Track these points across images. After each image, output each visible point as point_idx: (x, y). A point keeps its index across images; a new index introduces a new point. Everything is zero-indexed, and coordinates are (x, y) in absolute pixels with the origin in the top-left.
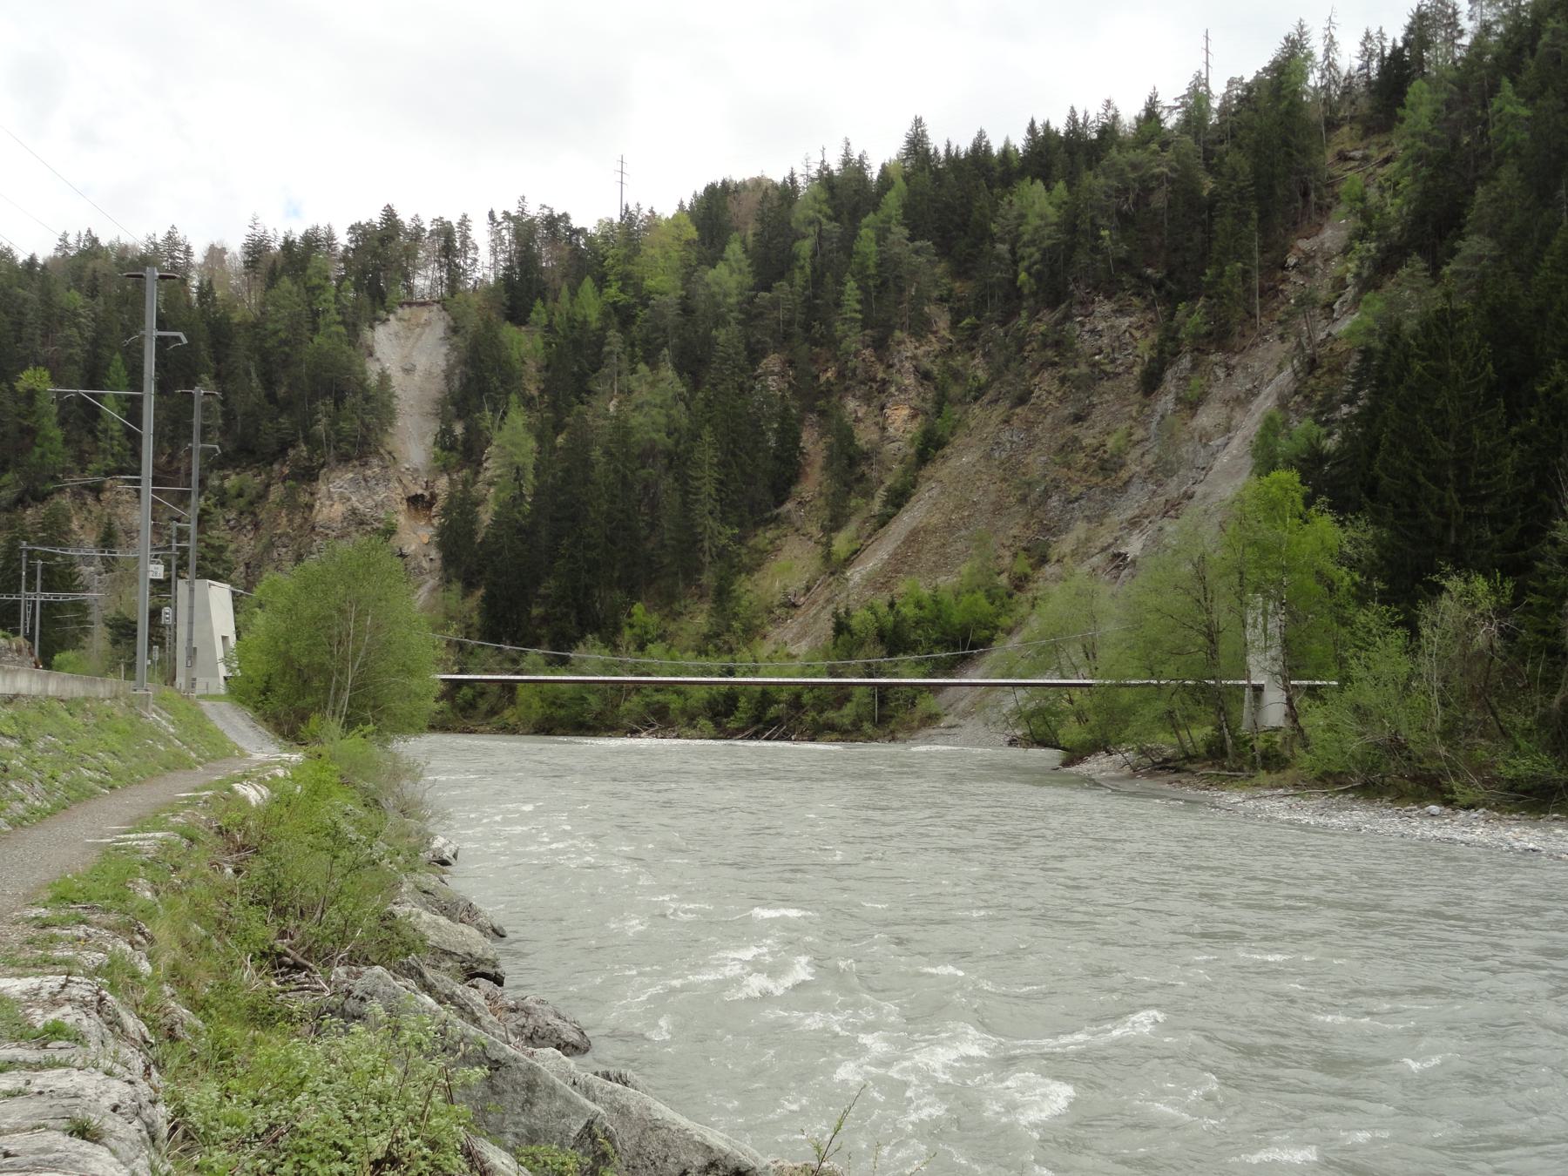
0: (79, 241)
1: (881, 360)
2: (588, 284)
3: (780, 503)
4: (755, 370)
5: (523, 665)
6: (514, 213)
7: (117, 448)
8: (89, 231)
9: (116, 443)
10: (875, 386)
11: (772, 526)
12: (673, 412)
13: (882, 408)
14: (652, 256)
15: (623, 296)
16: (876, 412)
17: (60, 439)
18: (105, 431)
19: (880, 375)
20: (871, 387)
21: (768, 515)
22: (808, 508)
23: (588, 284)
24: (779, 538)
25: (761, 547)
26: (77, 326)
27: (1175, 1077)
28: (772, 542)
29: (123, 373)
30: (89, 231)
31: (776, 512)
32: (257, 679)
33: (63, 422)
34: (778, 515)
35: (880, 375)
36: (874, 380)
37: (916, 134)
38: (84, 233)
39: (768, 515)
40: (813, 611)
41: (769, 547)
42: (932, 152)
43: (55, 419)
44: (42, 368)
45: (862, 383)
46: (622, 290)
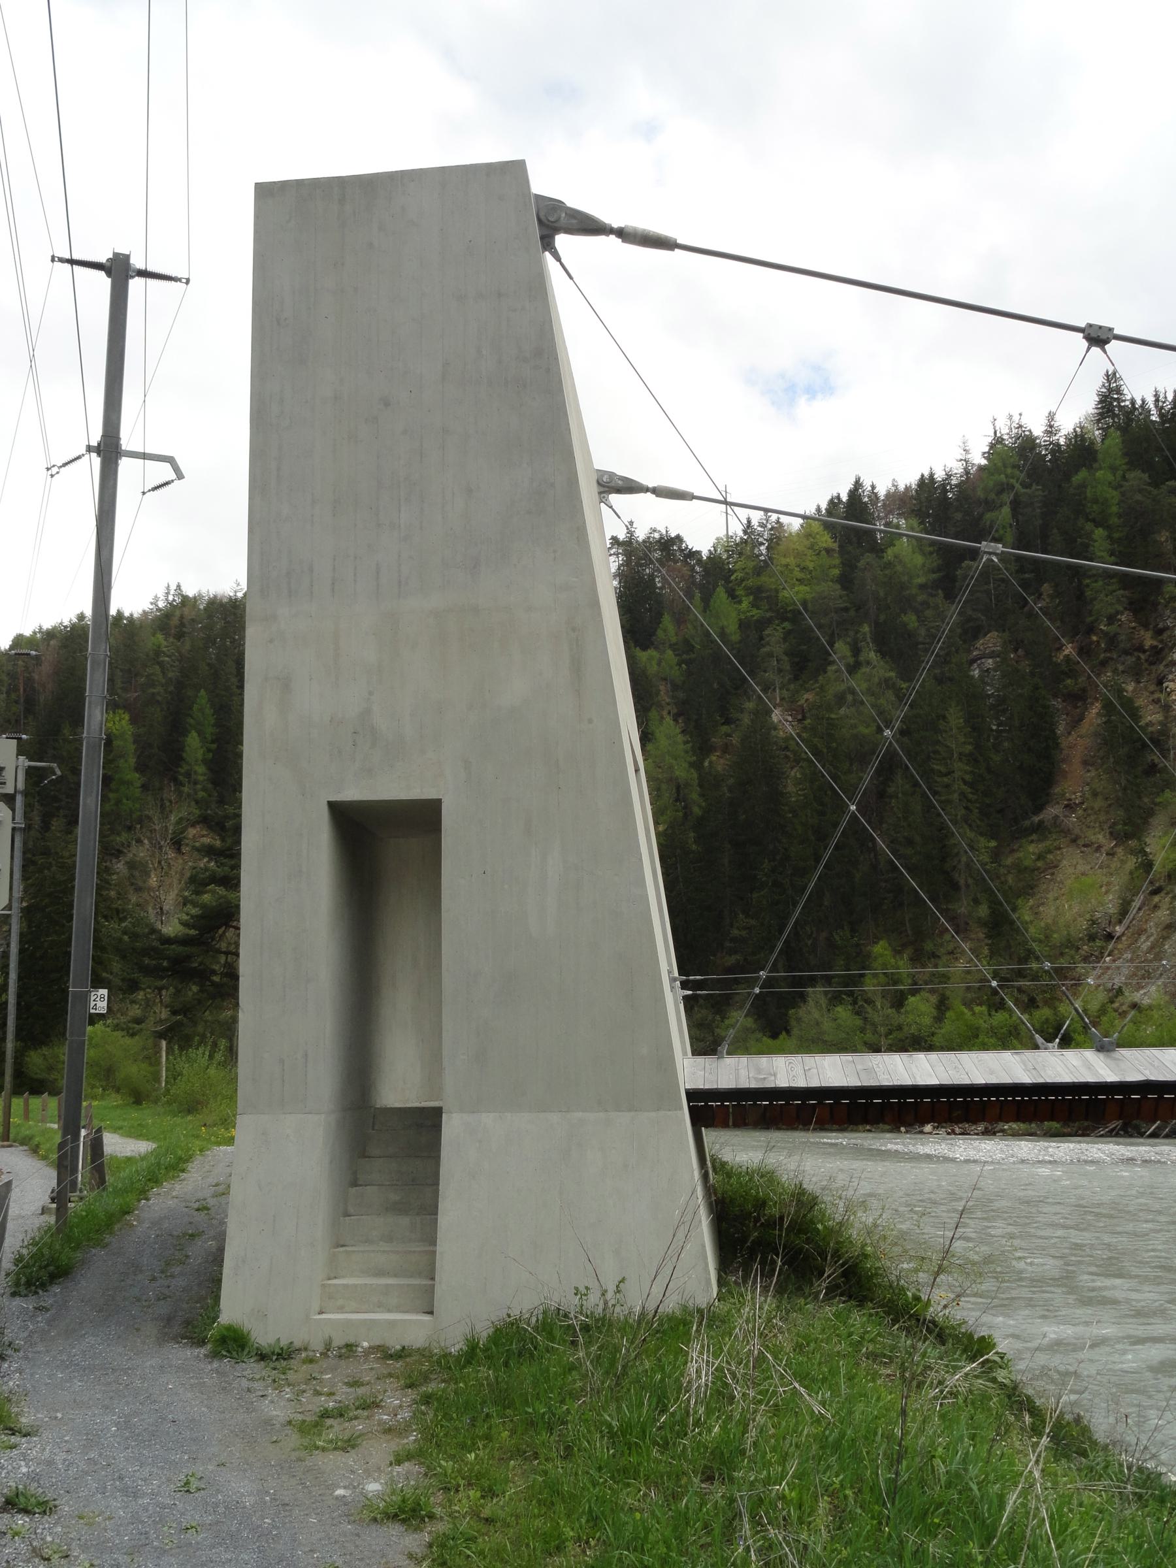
0: (168, 594)
1: (1146, 626)
2: (721, 593)
3: (1039, 809)
4: (969, 651)
5: (1072, 1008)
6: (622, 536)
7: (201, 794)
8: (179, 586)
9: (199, 786)
10: (1143, 657)
11: (1034, 837)
12: (882, 701)
13: (1160, 683)
14: (787, 566)
15: (755, 611)
16: (1152, 688)
17: (138, 784)
18: (188, 775)
19: (1149, 642)
20: (1139, 658)
21: (1027, 823)
22: (1080, 812)
23: (721, 593)
24: (1050, 852)
25: (1027, 863)
26: (161, 664)
27: (1002, 1314)
28: (1040, 857)
29: (208, 711)
30: (179, 586)
31: (1036, 819)
32: (1118, 462)
33: (141, 768)
34: (1041, 822)
35: (1149, 642)
36: (1140, 649)
37: (1110, 390)
38: (173, 587)
39: (1027, 823)
40: (1145, 944)
41: (1039, 864)
42: (935, 576)
43: (132, 761)
44: (121, 711)
45: (1126, 652)
46: (754, 605)
